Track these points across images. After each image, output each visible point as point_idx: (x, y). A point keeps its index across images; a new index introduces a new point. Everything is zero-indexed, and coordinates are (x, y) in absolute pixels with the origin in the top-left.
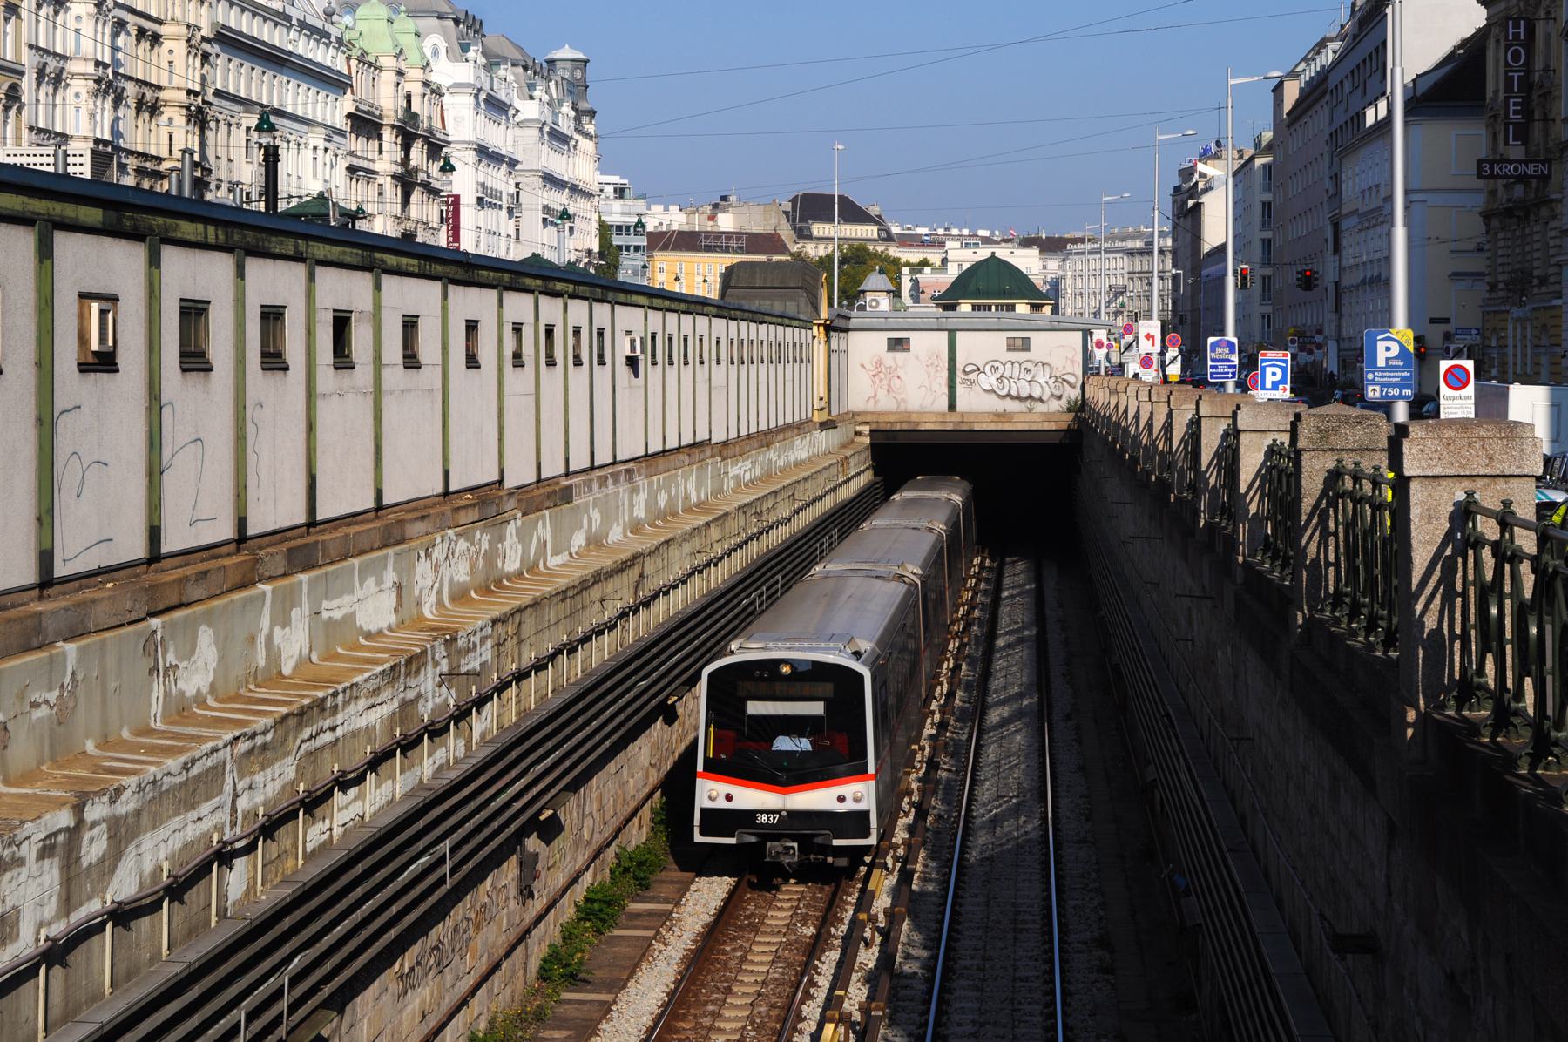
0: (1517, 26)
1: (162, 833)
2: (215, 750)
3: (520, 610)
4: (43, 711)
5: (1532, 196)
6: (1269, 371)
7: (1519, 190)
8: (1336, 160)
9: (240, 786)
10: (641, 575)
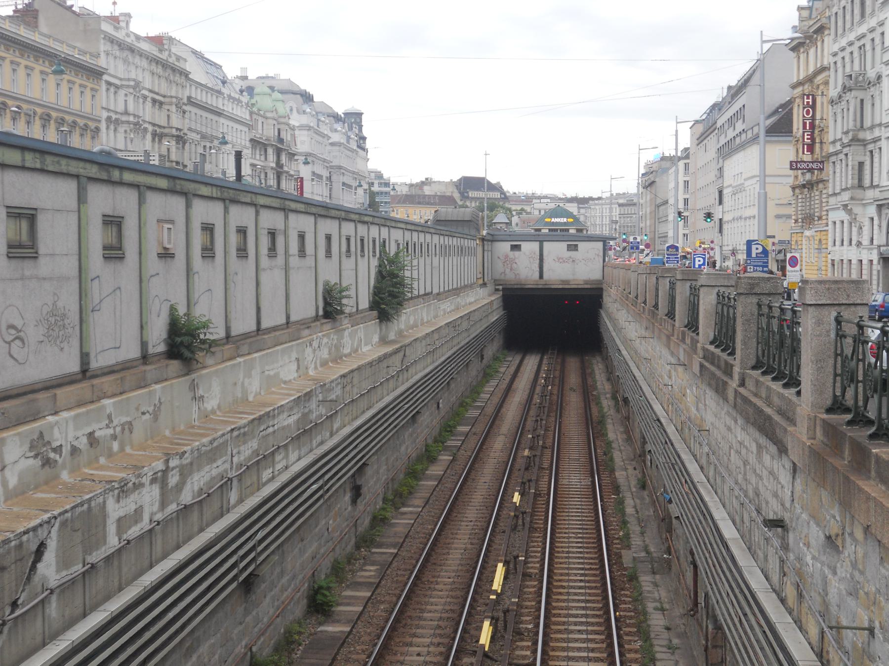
0: (808, 98)
1: (202, 473)
2: (223, 435)
3: (352, 371)
4: (147, 416)
5: (815, 178)
6: (697, 259)
7: (808, 176)
8: (721, 161)
9: (234, 452)
10: (404, 355)
